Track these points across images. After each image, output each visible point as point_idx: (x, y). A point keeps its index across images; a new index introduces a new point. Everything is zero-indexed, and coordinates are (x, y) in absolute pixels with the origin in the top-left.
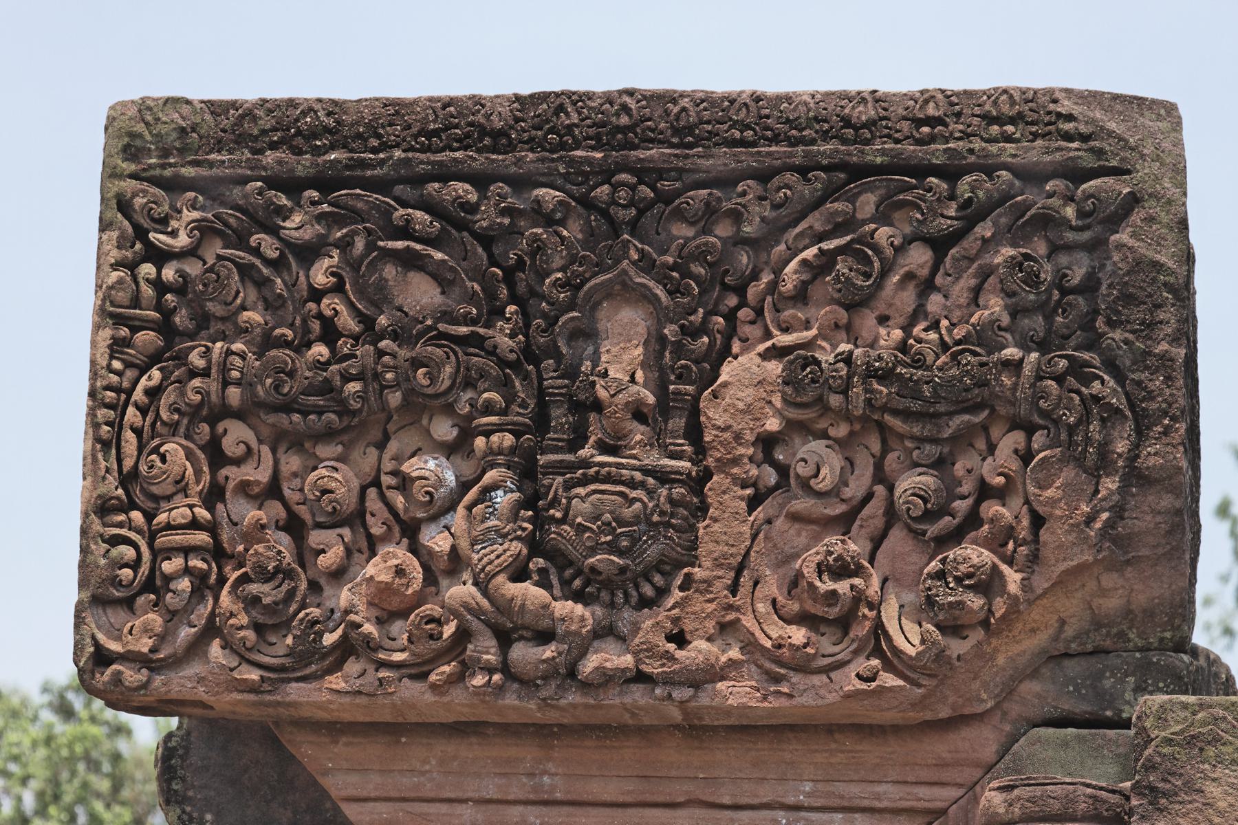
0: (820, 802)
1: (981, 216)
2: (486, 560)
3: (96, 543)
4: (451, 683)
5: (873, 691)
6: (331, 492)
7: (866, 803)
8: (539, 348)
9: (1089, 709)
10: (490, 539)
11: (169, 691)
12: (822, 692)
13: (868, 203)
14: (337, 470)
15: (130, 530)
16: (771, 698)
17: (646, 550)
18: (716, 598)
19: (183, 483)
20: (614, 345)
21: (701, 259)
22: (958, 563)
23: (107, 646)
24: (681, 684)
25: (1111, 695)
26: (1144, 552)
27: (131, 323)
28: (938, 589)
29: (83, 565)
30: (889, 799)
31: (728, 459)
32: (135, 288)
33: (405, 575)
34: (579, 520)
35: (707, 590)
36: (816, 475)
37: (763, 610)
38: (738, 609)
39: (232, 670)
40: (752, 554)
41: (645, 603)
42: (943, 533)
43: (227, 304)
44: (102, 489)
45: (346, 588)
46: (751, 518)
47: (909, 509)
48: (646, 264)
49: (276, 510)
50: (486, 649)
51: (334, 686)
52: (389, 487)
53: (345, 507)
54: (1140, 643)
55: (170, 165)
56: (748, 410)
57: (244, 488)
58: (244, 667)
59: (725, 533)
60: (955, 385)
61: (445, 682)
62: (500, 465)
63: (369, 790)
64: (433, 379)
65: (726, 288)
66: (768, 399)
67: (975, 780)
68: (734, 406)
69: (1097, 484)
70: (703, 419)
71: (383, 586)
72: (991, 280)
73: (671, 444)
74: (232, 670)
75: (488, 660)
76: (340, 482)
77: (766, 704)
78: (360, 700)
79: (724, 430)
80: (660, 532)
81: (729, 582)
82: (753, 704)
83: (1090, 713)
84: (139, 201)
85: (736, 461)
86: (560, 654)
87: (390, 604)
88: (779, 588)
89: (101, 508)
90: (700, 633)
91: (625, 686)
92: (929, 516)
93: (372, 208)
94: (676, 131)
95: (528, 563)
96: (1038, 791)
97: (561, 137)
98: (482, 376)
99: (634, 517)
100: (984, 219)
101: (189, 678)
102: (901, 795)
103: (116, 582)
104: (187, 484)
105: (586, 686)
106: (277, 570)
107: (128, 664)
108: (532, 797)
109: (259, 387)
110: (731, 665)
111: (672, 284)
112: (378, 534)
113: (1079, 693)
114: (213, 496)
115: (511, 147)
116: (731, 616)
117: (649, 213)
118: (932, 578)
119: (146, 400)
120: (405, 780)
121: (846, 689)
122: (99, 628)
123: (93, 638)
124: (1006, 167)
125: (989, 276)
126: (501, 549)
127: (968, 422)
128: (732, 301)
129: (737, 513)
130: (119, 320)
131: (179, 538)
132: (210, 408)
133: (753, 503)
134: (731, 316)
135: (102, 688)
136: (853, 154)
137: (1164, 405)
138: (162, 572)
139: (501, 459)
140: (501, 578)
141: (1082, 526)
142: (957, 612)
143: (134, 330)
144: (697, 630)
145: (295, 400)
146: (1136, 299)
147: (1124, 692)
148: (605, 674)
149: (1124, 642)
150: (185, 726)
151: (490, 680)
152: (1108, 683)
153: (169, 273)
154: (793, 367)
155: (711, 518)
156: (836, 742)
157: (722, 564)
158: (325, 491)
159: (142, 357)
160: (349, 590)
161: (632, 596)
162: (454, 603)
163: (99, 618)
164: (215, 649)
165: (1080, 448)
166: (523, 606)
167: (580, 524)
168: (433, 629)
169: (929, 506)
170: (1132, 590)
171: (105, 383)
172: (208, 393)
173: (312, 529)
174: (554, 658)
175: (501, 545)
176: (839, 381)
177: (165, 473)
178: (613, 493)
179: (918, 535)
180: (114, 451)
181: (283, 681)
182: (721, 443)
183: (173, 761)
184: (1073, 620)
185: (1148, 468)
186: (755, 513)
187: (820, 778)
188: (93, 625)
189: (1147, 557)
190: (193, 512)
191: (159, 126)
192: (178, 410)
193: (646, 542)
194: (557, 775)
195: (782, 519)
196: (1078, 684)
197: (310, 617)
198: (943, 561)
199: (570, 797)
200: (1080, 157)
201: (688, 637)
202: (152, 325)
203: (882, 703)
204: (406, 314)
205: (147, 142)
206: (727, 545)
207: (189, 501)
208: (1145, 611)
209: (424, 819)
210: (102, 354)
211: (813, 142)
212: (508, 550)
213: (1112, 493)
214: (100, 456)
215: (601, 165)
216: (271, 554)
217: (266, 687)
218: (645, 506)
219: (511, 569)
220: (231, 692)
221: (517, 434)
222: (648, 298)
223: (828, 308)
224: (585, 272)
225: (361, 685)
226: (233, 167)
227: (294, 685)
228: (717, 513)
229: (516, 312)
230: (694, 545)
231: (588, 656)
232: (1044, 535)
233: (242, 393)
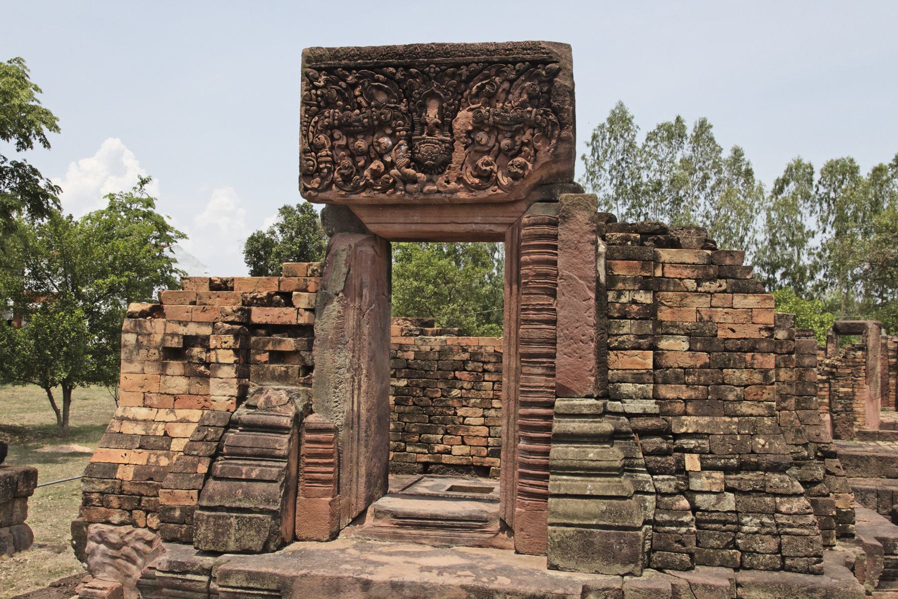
48: (438, 88)
94: (445, 53)
130: (307, 104)
133: (466, 148)
140: (404, 168)
143: (311, 107)
153: (319, 92)
179: (506, 155)
221: (407, 131)
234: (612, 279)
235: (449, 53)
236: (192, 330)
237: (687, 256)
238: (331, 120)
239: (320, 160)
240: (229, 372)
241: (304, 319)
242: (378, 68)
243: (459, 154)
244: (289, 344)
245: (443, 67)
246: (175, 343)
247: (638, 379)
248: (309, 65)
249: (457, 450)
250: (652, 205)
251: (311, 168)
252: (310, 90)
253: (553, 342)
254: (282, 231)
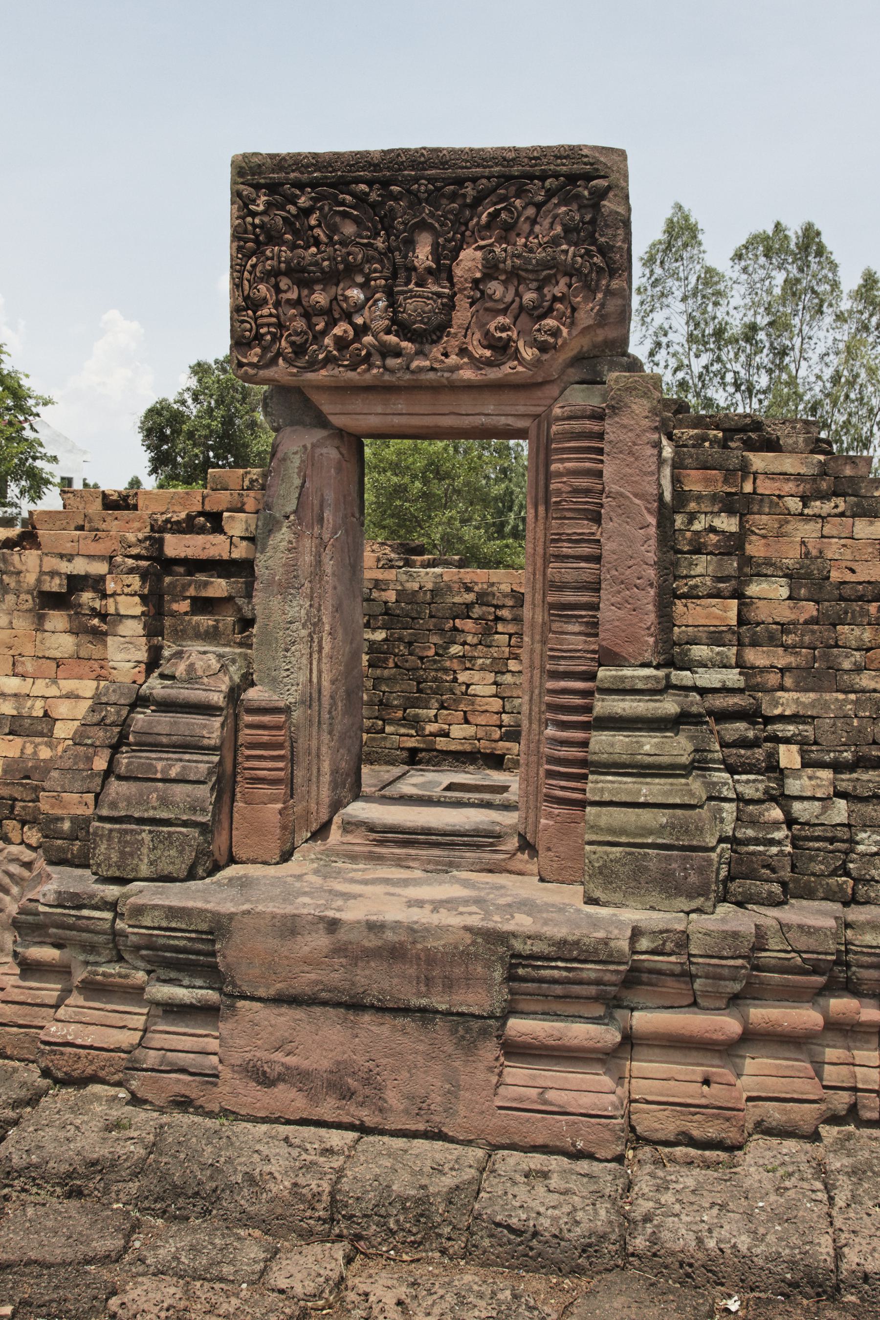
48: (432, 215)
130: (240, 239)
131: (265, 320)
133: (472, 304)
143: (246, 242)
179: (531, 315)
221: (386, 280)
232: (576, 314)
234: (681, 497)
235: (446, 162)
236: (80, 566)
237: (789, 464)
238: (275, 263)
239: (259, 321)
240: (133, 628)
241: (240, 552)
242: (342, 184)
243: (462, 314)
244: (219, 587)
245: (438, 184)
246: (55, 585)
247: (716, 639)
249: (457, 731)
253: (595, 587)
254: (196, 399)
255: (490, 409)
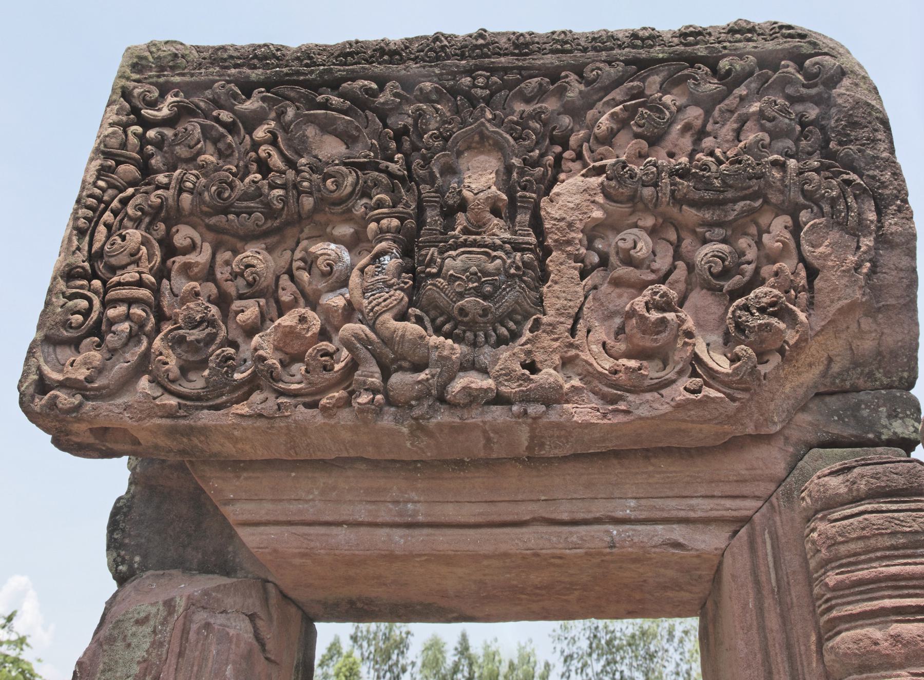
0: (644, 515)
1: (737, 84)
2: (375, 302)
3: (58, 298)
4: (338, 407)
5: (700, 401)
6: (253, 266)
7: (682, 514)
8: (418, 177)
9: (855, 433)
10: (378, 288)
11: (98, 415)
12: (656, 405)
13: (655, 81)
14: (259, 253)
15: (89, 291)
16: (610, 416)
17: (504, 296)
18: (560, 338)
19: (137, 257)
20: (474, 173)
21: (537, 117)
22: (760, 298)
23: (49, 375)
24: (536, 401)
25: (870, 421)
26: (892, 301)
27: (117, 158)
28: (744, 316)
29: (44, 314)
30: (702, 510)
31: (563, 240)
32: (124, 137)
33: (306, 321)
34: (451, 272)
35: (552, 332)
36: (635, 247)
37: (597, 350)
38: (577, 347)
39: (155, 398)
40: (585, 309)
41: (501, 341)
42: (736, 287)
43: (190, 147)
44: (71, 260)
45: (257, 336)
46: (584, 283)
47: (711, 267)
48: (498, 121)
49: (211, 288)
50: (371, 373)
51: (239, 412)
52: (299, 268)
53: (263, 279)
54: (885, 381)
55: (164, 76)
56: (577, 207)
57: (186, 269)
58: (166, 396)
59: (564, 292)
60: (740, 174)
61: (334, 406)
62: (387, 240)
63: (262, 515)
64: (338, 185)
65: (553, 141)
66: (592, 199)
67: (770, 492)
68: (566, 206)
69: (858, 242)
70: (543, 213)
71: (288, 329)
72: (748, 124)
73: (520, 230)
74: (155, 398)
75: (372, 382)
76: (260, 260)
77: (606, 421)
78: (260, 423)
79: (559, 220)
80: (516, 283)
81: (569, 327)
82: (594, 421)
83: (856, 436)
84: (137, 91)
85: (569, 242)
86: (433, 376)
87: (292, 347)
88: (608, 334)
89: (69, 274)
90: (548, 363)
91: (486, 408)
92: (725, 274)
93: (301, 97)
94: (516, 46)
95: (408, 309)
96: (879, 468)
97: (436, 53)
98: (375, 185)
99: (496, 269)
100: (739, 86)
101: (118, 406)
102: (712, 506)
103: (67, 325)
104: (140, 258)
105: (453, 405)
106: (203, 320)
107: (64, 390)
108: (397, 519)
109: (206, 194)
110: (573, 391)
111: (516, 133)
112: (287, 300)
113: (843, 421)
114: (162, 273)
115: (402, 61)
116: (573, 352)
117: (498, 95)
118: (741, 310)
119: (119, 206)
120: (291, 506)
121: (678, 398)
122: (46, 362)
123: (39, 368)
124: (749, 53)
125: (746, 122)
126: (387, 295)
127: (749, 205)
128: (558, 149)
129: (572, 278)
130: (107, 155)
131: (125, 292)
132: (167, 211)
133: (583, 274)
134: (559, 159)
135: (39, 411)
136: (643, 54)
137: (895, 192)
138: (106, 316)
139: (389, 236)
140: (387, 316)
141: (853, 271)
142: (765, 334)
143: (118, 163)
144: (546, 361)
145: (232, 205)
146: (861, 124)
147: (880, 418)
148: (470, 395)
149: (872, 382)
150: (132, 491)
151: (373, 398)
152: (865, 413)
153: (151, 133)
154: (615, 168)
155: (552, 281)
156: (653, 465)
157: (563, 313)
158: (248, 266)
159: (122, 181)
160: (261, 337)
161: (491, 336)
162: (347, 334)
163: (49, 355)
164: (144, 383)
165: (843, 214)
166: (403, 336)
167: (452, 275)
168: (327, 361)
169: (727, 263)
170: (883, 333)
171: (89, 193)
172: (167, 199)
173: (236, 300)
174: (428, 379)
175: (387, 293)
176: (651, 176)
177: (122, 247)
178: (478, 253)
179: (714, 290)
180: (87, 238)
181: (197, 408)
182: (558, 229)
183: (118, 517)
184: (838, 359)
185: (892, 234)
186: (586, 280)
187: (642, 495)
188: (41, 360)
189: (893, 305)
190: (140, 277)
191: (160, 53)
192: (141, 210)
193: (505, 289)
194: (419, 502)
195: (606, 285)
196: (841, 414)
197: (225, 353)
198: (747, 299)
199: (429, 519)
200: (801, 46)
201: (539, 366)
202: (133, 162)
203: (706, 413)
204: (320, 160)
205: (150, 62)
206: (566, 300)
207: (140, 269)
208: (891, 352)
209: (305, 539)
210: (91, 176)
211: (612, 49)
212: (393, 295)
213: (869, 248)
214: (75, 239)
215: (464, 67)
216: (199, 309)
217: (182, 412)
218: (504, 261)
219: (395, 311)
220: (152, 417)
221: (402, 220)
222: (499, 147)
223: (634, 142)
224: (453, 128)
225: (262, 408)
226: (207, 75)
227: (206, 411)
228: (557, 278)
229: (402, 158)
230: (540, 301)
231: (456, 380)
232: (818, 283)
233: (192, 200)
235: (527, 45)
238: (170, 194)
239: (112, 294)
245: (510, 77)
248: (137, 76)
250: (627, 661)
251: (196, 594)
252: (125, 126)
255: (628, 507)
